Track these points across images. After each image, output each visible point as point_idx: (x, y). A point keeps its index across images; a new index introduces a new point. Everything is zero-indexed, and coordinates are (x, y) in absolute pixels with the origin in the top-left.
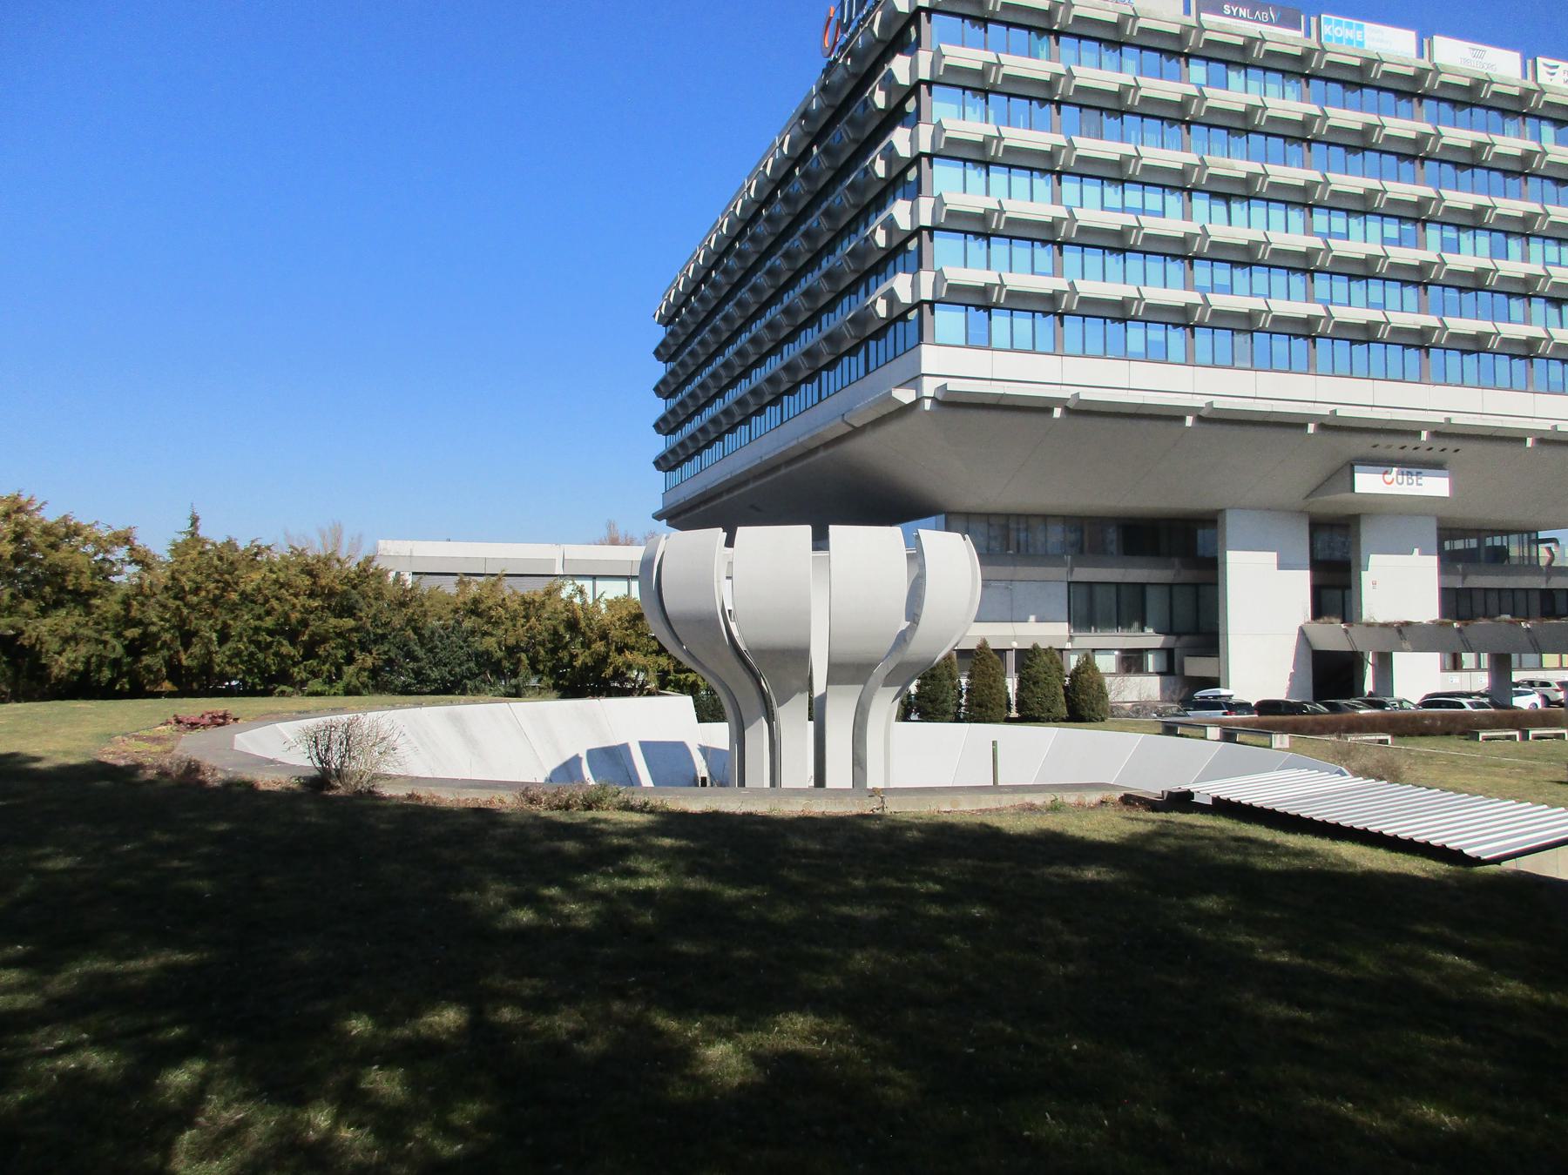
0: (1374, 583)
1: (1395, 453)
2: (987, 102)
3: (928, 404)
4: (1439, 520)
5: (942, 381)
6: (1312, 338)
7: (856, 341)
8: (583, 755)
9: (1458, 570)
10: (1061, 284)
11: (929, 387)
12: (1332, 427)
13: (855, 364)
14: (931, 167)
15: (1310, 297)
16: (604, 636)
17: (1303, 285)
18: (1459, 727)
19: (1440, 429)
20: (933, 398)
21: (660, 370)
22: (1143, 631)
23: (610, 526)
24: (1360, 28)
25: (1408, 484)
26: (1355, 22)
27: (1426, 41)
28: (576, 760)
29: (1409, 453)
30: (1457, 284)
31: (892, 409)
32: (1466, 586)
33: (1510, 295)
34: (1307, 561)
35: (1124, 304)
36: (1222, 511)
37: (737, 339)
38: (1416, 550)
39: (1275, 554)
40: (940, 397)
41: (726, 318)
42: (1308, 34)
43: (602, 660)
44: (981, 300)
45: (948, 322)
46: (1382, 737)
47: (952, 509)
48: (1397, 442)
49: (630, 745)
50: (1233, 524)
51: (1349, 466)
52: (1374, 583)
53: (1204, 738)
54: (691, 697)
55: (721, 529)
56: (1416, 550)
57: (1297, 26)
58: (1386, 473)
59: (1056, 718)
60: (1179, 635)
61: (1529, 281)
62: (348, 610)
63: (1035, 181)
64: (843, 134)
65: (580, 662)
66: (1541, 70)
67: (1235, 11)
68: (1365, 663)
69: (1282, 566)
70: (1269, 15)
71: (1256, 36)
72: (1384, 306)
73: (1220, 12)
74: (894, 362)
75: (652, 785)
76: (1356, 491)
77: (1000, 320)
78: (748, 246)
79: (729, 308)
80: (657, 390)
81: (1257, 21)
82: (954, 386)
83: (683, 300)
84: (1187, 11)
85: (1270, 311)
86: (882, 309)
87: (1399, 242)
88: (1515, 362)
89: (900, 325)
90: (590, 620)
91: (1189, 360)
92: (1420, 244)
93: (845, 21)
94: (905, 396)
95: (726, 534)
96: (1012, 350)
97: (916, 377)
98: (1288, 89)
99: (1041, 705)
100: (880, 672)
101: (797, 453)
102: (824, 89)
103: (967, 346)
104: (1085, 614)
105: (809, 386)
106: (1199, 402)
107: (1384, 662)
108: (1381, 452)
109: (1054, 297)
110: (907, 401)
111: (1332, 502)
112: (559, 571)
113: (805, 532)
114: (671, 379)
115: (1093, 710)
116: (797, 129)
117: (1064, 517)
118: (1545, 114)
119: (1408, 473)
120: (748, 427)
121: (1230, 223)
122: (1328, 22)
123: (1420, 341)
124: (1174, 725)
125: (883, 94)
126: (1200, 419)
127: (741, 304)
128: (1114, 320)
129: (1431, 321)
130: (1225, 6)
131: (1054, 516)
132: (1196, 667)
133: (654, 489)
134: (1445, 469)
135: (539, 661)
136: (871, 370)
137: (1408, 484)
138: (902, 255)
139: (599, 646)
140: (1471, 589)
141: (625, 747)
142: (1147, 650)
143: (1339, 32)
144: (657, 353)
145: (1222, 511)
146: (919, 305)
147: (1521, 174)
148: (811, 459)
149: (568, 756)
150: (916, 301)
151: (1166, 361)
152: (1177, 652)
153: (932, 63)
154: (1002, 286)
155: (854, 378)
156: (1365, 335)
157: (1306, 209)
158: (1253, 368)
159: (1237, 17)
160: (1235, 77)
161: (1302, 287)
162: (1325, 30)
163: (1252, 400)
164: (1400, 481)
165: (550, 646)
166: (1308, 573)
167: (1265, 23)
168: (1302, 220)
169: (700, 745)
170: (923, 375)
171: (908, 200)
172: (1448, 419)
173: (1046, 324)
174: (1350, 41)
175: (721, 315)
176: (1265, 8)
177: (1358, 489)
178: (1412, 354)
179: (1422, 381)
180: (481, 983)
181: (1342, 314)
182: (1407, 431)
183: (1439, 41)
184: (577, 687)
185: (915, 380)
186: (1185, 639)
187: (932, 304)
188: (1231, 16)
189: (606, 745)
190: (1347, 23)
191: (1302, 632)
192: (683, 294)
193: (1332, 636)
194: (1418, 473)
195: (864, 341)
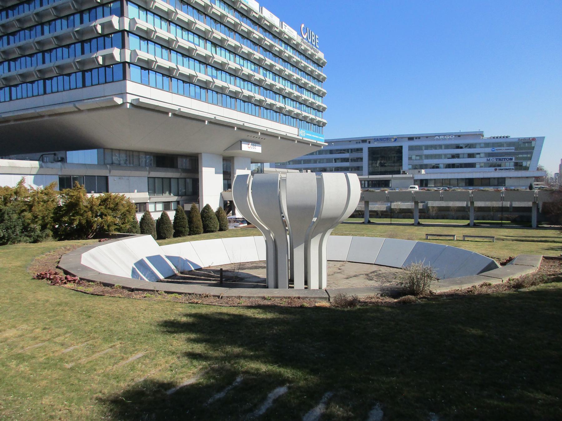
1: (252, 139)
4: (251, 159)
5: (138, 97)
8: (135, 267)
9: (107, 168)
11: (130, 98)
12: (242, 129)
14: (127, 5)
20: (131, 104)
22: (170, 195)
29: (255, 139)
30: (200, 85)
31: (113, 104)
36: (201, 153)
40: (135, 103)
45: (134, 72)
47: (105, 147)
48: (253, 135)
49: (144, 259)
50: (204, 159)
51: (240, 142)
58: (249, 144)
60: (182, 196)
66: (284, 26)
75: (131, 277)
76: (242, 150)
82: (142, 100)
94: (119, 101)
104: (152, 190)
110: (119, 103)
111: (229, 153)
117: (144, 152)
119: (253, 145)
142: (172, 202)
145: (201, 153)
149: (131, 268)
150: (123, 61)
152: (180, 202)
157: (168, 22)
166: (222, 175)
168: (203, 44)
170: (127, 93)
172: (215, 117)
177: (243, 149)
180: (154, 398)
183: (264, 9)
184: (58, 228)
185: (123, 94)
186: (183, 197)
187: (129, 63)
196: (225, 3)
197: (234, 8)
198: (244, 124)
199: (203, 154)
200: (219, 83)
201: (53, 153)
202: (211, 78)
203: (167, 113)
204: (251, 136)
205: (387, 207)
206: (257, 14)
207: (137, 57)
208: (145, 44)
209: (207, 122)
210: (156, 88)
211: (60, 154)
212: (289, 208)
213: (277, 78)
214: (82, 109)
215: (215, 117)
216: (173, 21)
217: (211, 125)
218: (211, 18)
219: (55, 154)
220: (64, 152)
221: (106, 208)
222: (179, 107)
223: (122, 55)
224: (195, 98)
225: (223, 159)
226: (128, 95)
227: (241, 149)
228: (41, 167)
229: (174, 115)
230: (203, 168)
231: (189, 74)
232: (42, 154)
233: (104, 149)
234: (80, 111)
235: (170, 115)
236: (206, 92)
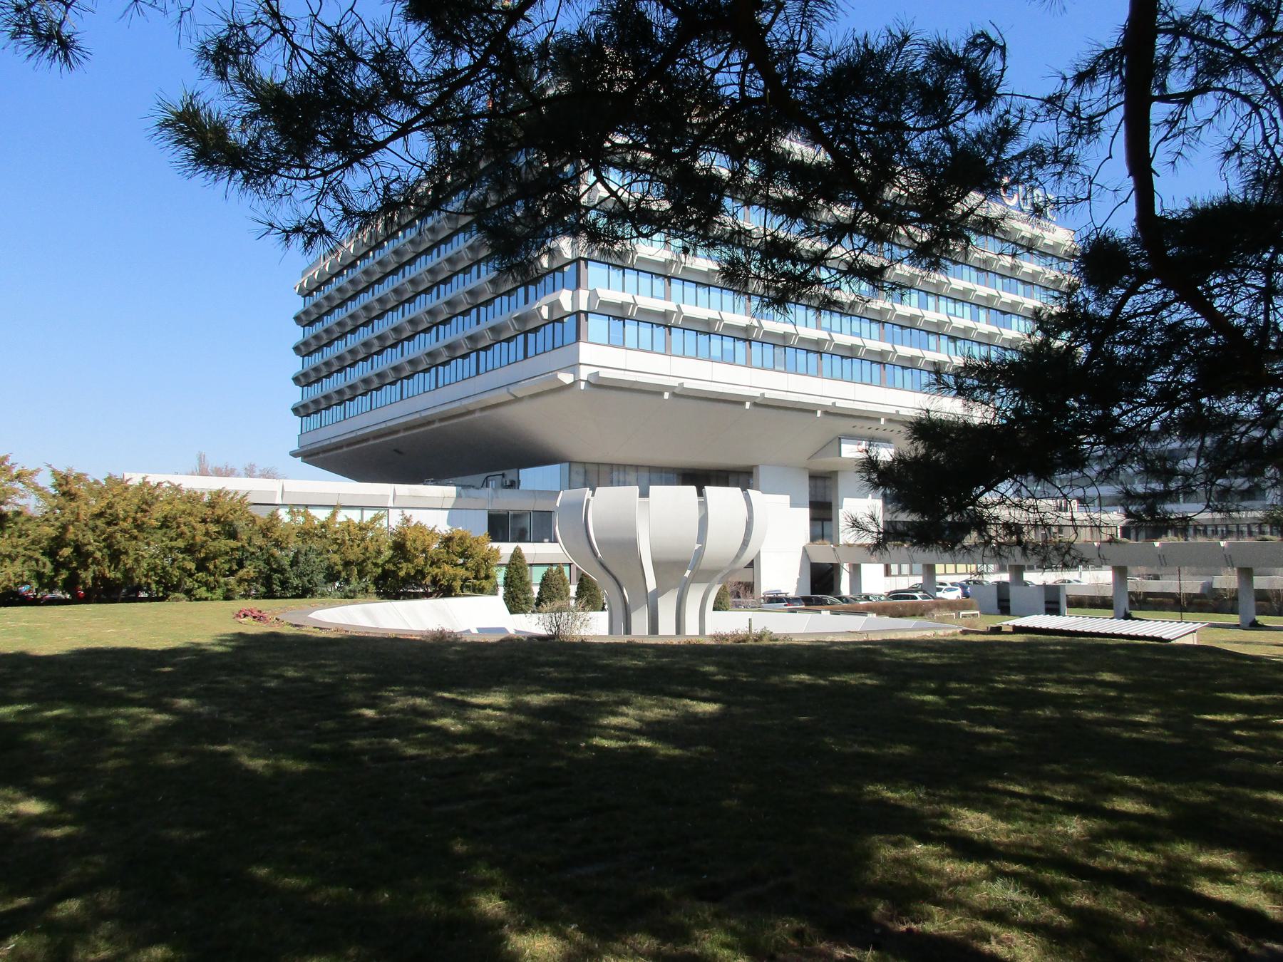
5: (595, 370)
6: (749, 341)
10: (671, 306)
11: (584, 373)
15: (818, 327)
18: (920, 611)
19: (892, 417)
23: (201, 459)
29: (873, 432)
33: (928, 332)
34: (806, 499)
35: (709, 322)
36: (756, 466)
40: (592, 381)
44: (619, 314)
45: (596, 326)
48: (867, 424)
61: (940, 324)
62: (233, 535)
69: (793, 505)
72: (860, 335)
77: (631, 327)
82: (604, 373)
85: (722, 320)
86: (545, 313)
88: (811, 355)
91: (748, 364)
94: (567, 378)
101: (459, 412)
103: (609, 345)
106: (674, 382)
107: (856, 570)
108: (858, 431)
109: (666, 314)
111: (824, 464)
112: (278, 501)
113: (694, 488)
123: (880, 359)
126: (755, 404)
128: (615, 318)
129: (887, 346)
131: (631, 466)
133: (290, 431)
145: (756, 466)
146: (577, 313)
147: (1031, 283)
148: (467, 418)
154: (635, 304)
156: (850, 353)
161: (742, 305)
166: (808, 510)
172: (897, 411)
173: (660, 332)
178: (876, 367)
181: (690, 310)
182: (871, 418)
185: (574, 366)
187: (586, 313)
191: (804, 549)
193: (823, 555)
198: (834, 403)
199: (761, 468)
201: (501, 472)
203: (815, 412)
205: (1203, 586)
209: (883, 420)
210: (638, 349)
211: (510, 474)
212: (657, 565)
213: (931, 300)
214: (519, 395)
215: (897, 411)
217: (758, 409)
219: (503, 475)
220: (516, 470)
221: (448, 552)
222: (834, 400)
223: (575, 299)
227: (840, 455)
228: (459, 495)
229: (755, 404)
232: (485, 475)
233: (571, 462)
234: (517, 400)
235: (666, 395)
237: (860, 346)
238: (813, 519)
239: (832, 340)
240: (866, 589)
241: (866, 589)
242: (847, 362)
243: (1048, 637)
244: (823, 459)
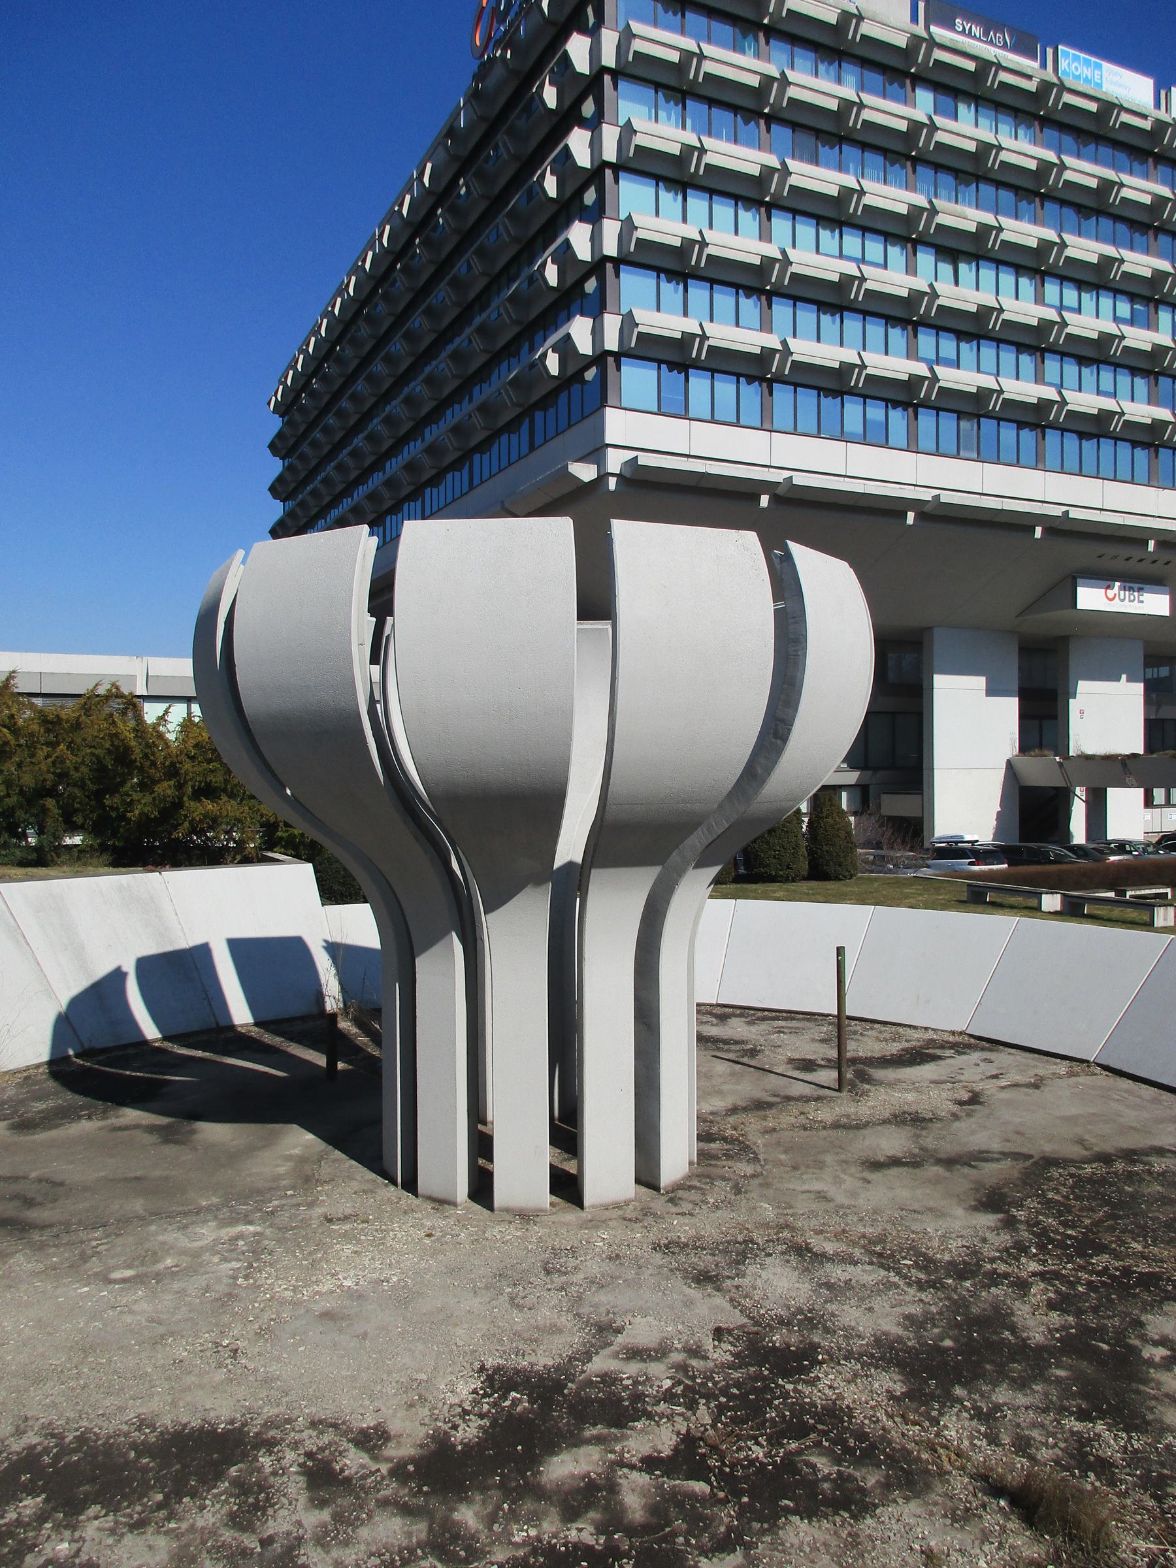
0: (1082, 712)
1: (1120, 565)
2: (684, 108)
3: (612, 483)
7: (518, 410)
8: (130, 968)
11: (615, 461)
13: (517, 441)
15: (1039, 379)
16: (172, 771)
17: (1033, 365)
19: (1056, 524)
21: (276, 466)
24: (1099, 67)
25: (1130, 601)
26: (1093, 59)
27: (1163, 93)
28: (118, 976)
31: (567, 489)
32: (1159, 717)
34: (1015, 685)
36: (929, 629)
37: (368, 479)
38: (1124, 677)
39: (984, 678)
40: (628, 474)
41: (354, 454)
42: (1044, 65)
43: (171, 811)
46: (1161, 891)
48: (1124, 551)
49: (213, 946)
50: (941, 643)
52: (1082, 712)
53: (1149, 925)
54: (309, 867)
55: (365, 528)
56: (1124, 677)
57: (1032, 55)
58: (1108, 587)
59: (797, 876)
60: (875, 769)
63: (741, 212)
64: (504, 147)
65: (137, 812)
67: (967, 28)
68: (1071, 794)
69: (991, 691)
70: (1004, 37)
71: (990, 59)
73: (951, 27)
74: (567, 433)
76: (1079, 607)
77: (699, 383)
78: (382, 308)
79: (358, 441)
80: (272, 489)
81: (991, 43)
82: (645, 460)
83: (303, 383)
84: (914, 18)
87: (1132, 322)
89: (576, 388)
90: (150, 747)
91: (912, 446)
92: (1151, 325)
93: (502, 8)
94: (585, 472)
95: (375, 540)
96: (713, 421)
97: (597, 450)
98: (1021, 132)
99: (778, 859)
100: (697, 841)
102: (475, 96)
103: (659, 413)
105: (457, 474)
111: (1047, 620)
114: (289, 477)
115: (840, 866)
116: (441, 154)
118: (1122, 287)
120: (381, 529)
121: (957, 283)
122: (1067, 55)
124: (982, 890)
125: (554, 90)
127: (372, 438)
130: (957, 21)
132: (897, 805)
134: (1165, 585)
135: (76, 811)
136: (537, 445)
137: (1130, 601)
138: (579, 301)
139: (166, 788)
140: (1163, 720)
141: (204, 950)
143: (1076, 68)
144: (272, 447)
145: (929, 629)
149: (102, 969)
151: (886, 445)
152: (872, 790)
153: (618, 47)
155: (514, 457)
157: (1038, 277)
158: (979, 459)
159: (970, 35)
160: (965, 111)
162: (1063, 64)
163: (978, 496)
164: (1122, 597)
165: (92, 787)
166: (1016, 700)
167: (999, 47)
168: (1033, 288)
169: (326, 941)
171: (588, 222)
173: (751, 393)
174: (1087, 80)
175: (349, 449)
176: (999, 28)
179: (1151, 483)
182: (1131, 538)
185: (596, 452)
186: (881, 774)
188: (963, 32)
189: (169, 948)
190: (1085, 60)
192: (301, 374)
194: (1140, 590)
195: (528, 411)
196: (712, 13)
197: (1037, 117)
200: (1085, 401)
202: (993, 378)
204: (1115, 557)
206: (1144, 117)
207: (636, 331)
208: (971, 350)
209: (1151, 544)
216: (780, 203)
218: (1063, 203)
224: (864, 440)
225: (1021, 649)
226: (610, 451)
230: (935, 676)
231: (978, 387)
236: (766, 391)
237: (993, 391)
238: (1025, 716)
239: (1064, 402)
240: (1116, 830)
241: (1116, 830)
242: (1089, 446)
243: (1138, 893)
244: (1059, 613)
